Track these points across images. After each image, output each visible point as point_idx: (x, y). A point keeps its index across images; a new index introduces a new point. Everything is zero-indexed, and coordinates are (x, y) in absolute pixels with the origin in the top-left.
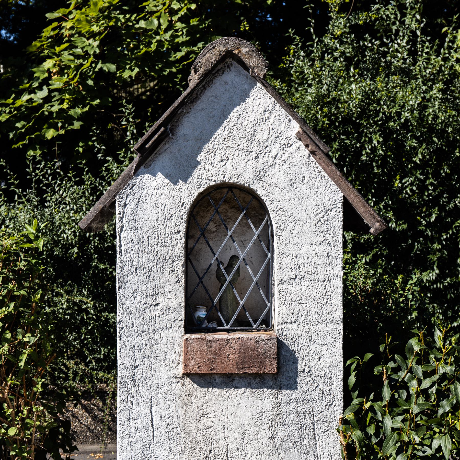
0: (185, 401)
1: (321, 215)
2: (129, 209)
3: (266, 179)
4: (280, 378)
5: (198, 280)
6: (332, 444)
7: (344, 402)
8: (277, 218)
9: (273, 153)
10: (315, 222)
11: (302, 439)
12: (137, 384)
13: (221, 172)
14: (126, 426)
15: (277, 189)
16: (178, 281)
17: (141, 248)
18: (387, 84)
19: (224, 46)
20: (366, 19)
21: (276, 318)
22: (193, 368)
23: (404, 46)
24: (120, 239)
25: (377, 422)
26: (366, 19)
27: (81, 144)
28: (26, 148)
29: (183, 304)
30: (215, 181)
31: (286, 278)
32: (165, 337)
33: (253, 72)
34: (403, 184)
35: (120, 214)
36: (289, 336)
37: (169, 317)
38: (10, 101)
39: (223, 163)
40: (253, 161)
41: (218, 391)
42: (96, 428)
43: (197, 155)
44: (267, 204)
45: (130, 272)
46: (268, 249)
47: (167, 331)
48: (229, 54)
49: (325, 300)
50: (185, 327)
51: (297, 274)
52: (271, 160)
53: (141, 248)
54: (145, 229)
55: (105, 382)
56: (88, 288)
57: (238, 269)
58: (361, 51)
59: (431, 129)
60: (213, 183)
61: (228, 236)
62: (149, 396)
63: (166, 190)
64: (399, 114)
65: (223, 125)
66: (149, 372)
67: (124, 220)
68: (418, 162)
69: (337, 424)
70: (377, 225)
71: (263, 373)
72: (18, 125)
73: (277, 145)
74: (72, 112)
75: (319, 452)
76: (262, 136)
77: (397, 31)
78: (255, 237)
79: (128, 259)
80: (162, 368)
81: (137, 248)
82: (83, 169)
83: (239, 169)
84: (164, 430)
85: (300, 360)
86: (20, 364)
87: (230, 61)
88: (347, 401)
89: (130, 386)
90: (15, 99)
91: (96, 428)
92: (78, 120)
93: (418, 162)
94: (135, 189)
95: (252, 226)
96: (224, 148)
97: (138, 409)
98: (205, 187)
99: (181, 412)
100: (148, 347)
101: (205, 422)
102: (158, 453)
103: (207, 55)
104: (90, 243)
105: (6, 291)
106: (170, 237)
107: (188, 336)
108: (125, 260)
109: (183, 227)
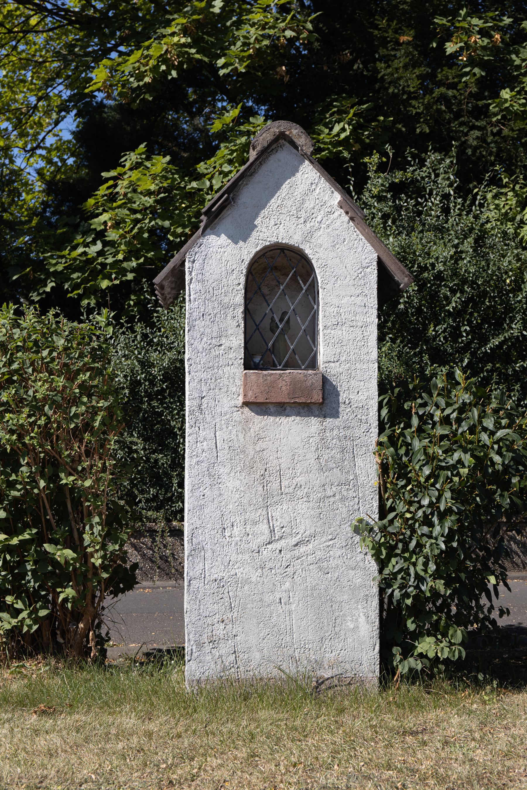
0: (245, 427)
1: (359, 271)
2: (197, 265)
3: (313, 240)
4: (325, 409)
5: (255, 327)
6: (369, 465)
7: (379, 429)
8: (322, 274)
9: (319, 219)
10: (354, 277)
11: (343, 461)
12: (203, 412)
13: (275, 234)
14: (194, 447)
15: (322, 249)
16: (238, 326)
17: (207, 297)
18: (421, 239)
19: (278, 128)
20: (402, 178)
21: (321, 359)
22: (251, 398)
23: (437, 204)
24: (189, 290)
25: (408, 445)
26: (402, 178)
27: (133, 297)
28: (81, 297)
29: (243, 345)
30: (270, 241)
31: (330, 324)
32: (227, 373)
33: (302, 150)
34: (437, 332)
35: (189, 268)
36: (332, 373)
37: (231, 356)
38: (67, 252)
39: (276, 227)
40: (302, 225)
41: (272, 418)
42: (145, 565)
43: (255, 219)
44: (313, 262)
45: (198, 317)
46: (315, 303)
47: (229, 368)
48: (281, 136)
49: (363, 343)
50: (244, 364)
51: (339, 320)
52: (317, 225)
53: (207, 297)
54: (211, 281)
55: (154, 522)
56: (139, 431)
57: (289, 318)
58: (398, 209)
59: (464, 281)
60: (268, 243)
61: (281, 290)
62: (214, 422)
63: (229, 249)
64: (433, 265)
65: (277, 195)
66: (213, 402)
67: (193, 274)
68: (451, 310)
69: (373, 447)
70: (406, 279)
71: (311, 403)
72: (75, 276)
73: (322, 212)
74: (125, 265)
75: (358, 472)
76: (309, 204)
77: (431, 191)
78: (304, 291)
79: (196, 307)
80: (224, 399)
81: (203, 297)
82: (135, 316)
83: (290, 232)
84: (226, 452)
85: (341, 393)
86: (95, 425)
87: (282, 141)
88: (381, 429)
89: (197, 414)
90: (71, 251)
91: (145, 565)
92: (131, 272)
93: (451, 310)
94: (203, 248)
95: (301, 282)
96: (278, 214)
97: (205, 433)
98: (262, 247)
99: (241, 436)
100: (213, 381)
101: (261, 445)
102: (221, 471)
103: (264, 135)
104: (141, 386)
105: (82, 363)
106: (231, 288)
107: (246, 371)
108: (194, 307)
109: (243, 280)
